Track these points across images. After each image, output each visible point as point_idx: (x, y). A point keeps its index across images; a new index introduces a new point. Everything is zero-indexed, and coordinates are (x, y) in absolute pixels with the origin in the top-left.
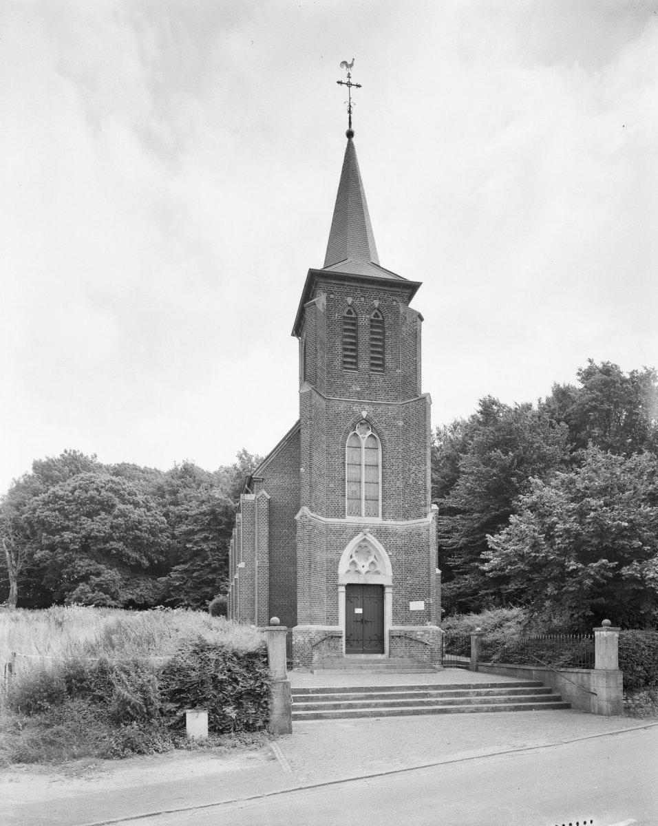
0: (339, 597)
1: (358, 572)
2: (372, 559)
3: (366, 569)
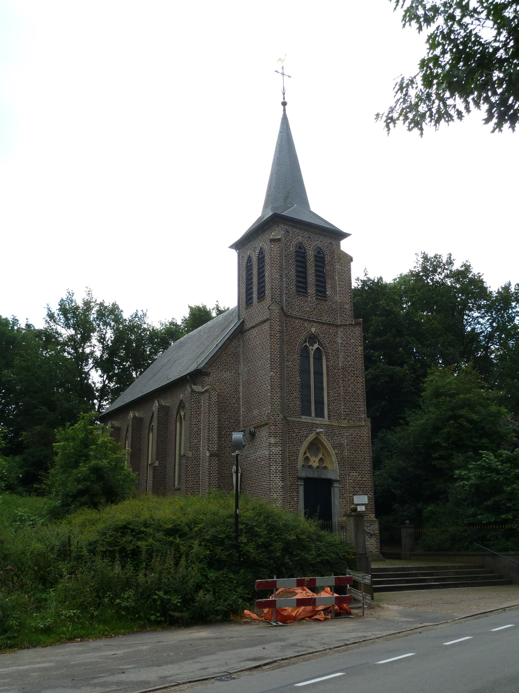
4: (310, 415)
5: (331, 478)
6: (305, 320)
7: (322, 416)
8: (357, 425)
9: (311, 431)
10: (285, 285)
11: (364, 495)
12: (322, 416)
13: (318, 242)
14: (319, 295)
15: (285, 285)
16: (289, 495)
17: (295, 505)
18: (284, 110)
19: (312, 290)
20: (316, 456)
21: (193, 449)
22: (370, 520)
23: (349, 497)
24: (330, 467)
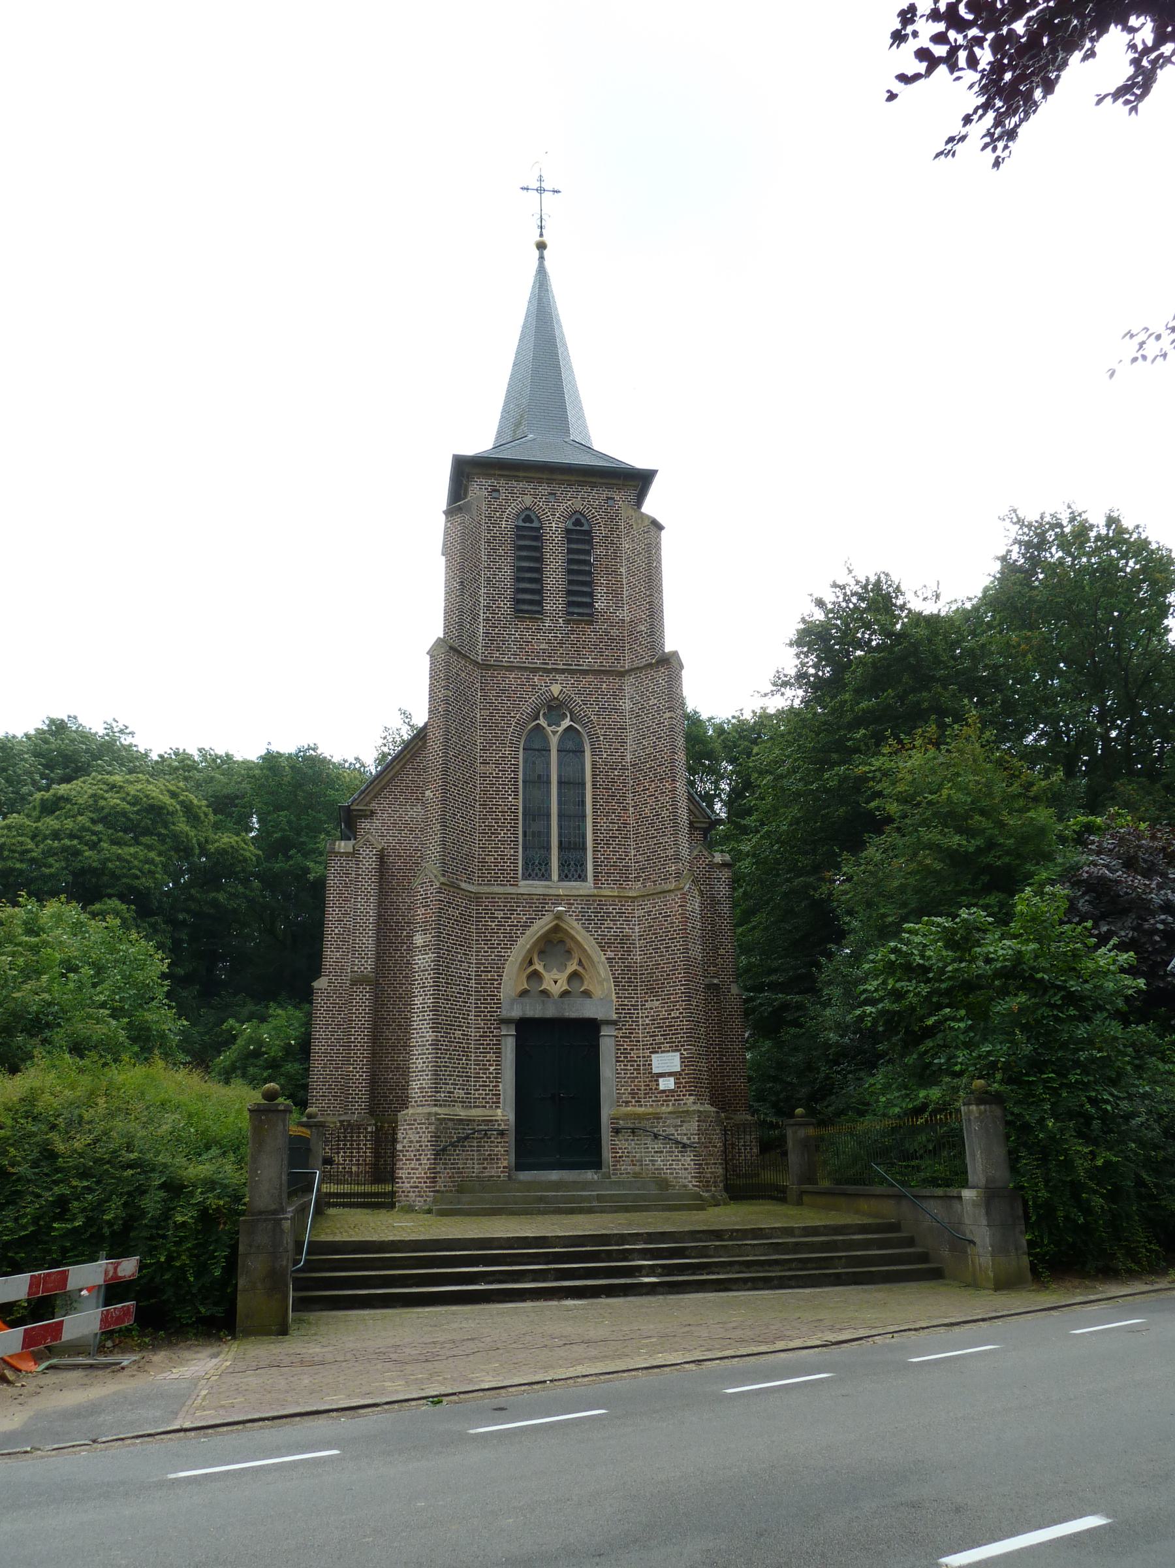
0: (503, 1047)
1: (545, 993)
2: (573, 967)
3: (562, 985)
4: (546, 876)
5: (592, 1016)
6: (534, 670)
8: (659, 890)
9: (540, 912)
10: (483, 603)
11: (673, 1051)
12: (582, 877)
13: (574, 500)
14: (574, 613)
15: (483, 603)
16: (475, 1060)
18: (542, 258)
19: (554, 603)
20: (562, 967)
22: (683, 1112)
23: (644, 1057)
24: (597, 992)
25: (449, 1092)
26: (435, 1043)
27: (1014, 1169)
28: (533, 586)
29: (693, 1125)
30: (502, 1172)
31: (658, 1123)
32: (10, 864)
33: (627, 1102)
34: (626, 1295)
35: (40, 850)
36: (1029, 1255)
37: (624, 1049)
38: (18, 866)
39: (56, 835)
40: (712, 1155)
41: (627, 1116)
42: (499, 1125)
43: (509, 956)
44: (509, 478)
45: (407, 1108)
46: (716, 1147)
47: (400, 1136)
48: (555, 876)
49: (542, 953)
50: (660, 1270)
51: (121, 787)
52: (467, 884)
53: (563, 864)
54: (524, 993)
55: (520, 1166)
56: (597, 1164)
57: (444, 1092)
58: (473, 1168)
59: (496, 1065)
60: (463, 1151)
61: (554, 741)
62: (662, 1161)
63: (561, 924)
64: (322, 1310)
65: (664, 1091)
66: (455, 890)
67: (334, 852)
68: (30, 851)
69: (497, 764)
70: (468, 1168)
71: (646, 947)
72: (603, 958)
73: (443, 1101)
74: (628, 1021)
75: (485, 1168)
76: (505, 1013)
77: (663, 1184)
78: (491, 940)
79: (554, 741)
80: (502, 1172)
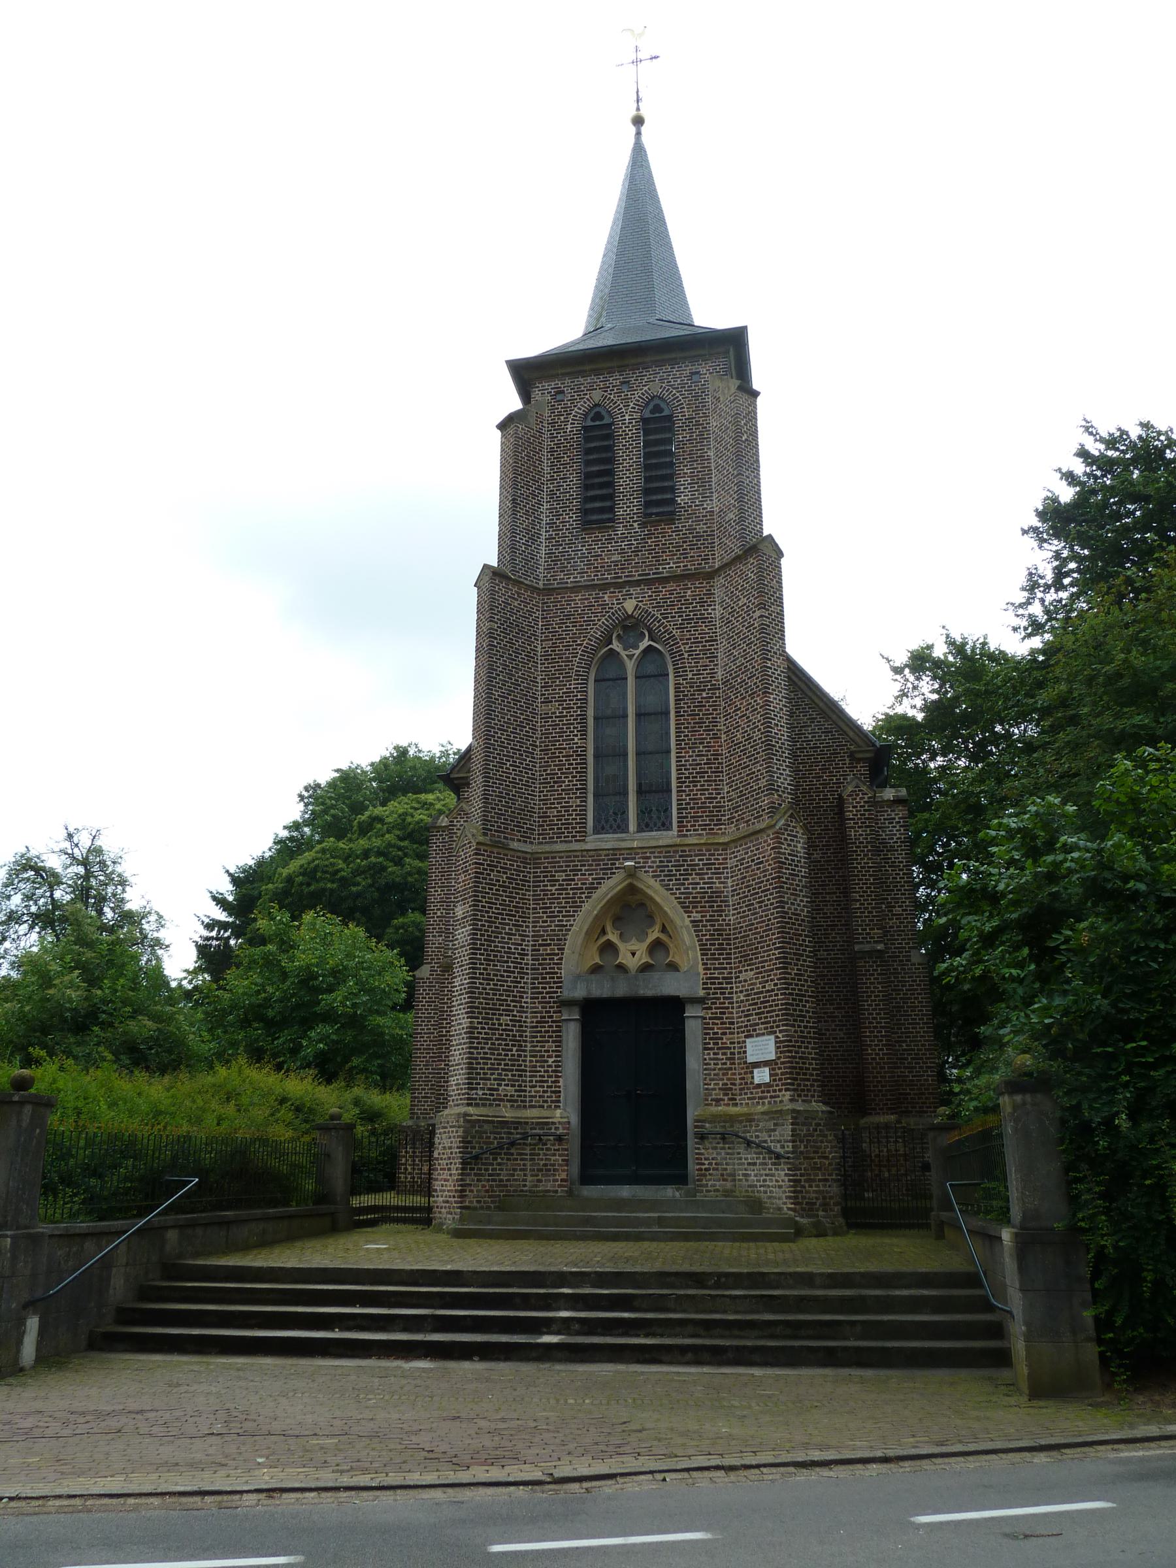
0: (564, 1034)
1: (621, 968)
2: (654, 934)
3: (642, 957)
4: (622, 828)
6: (604, 587)
7: (663, 824)
8: (751, 831)
9: (609, 871)
12: (666, 826)
14: (652, 514)
16: (531, 1051)
17: (549, 1076)
18: (638, 134)
19: (628, 506)
20: (642, 937)
21: (432, 959)
22: (776, 1112)
23: (739, 1043)
25: (489, 1089)
26: (471, 1030)
27: (1073, 1200)
28: (604, 492)
29: (787, 1130)
30: (560, 1186)
31: (751, 1126)
32: (322, 884)
33: (718, 1101)
34: (507, 1359)
35: (350, 870)
36: (1100, 1341)
37: (714, 1033)
38: (329, 885)
39: (366, 854)
40: (819, 1169)
41: (714, 1118)
42: (557, 1129)
43: (571, 925)
44: (573, 375)
45: (446, 1108)
46: (826, 1158)
47: (436, 1141)
48: (632, 827)
49: (618, 920)
50: (577, 1326)
51: (431, 804)
52: (522, 844)
53: (642, 812)
54: (596, 969)
55: (586, 1179)
56: (681, 1179)
57: (483, 1089)
58: (525, 1180)
59: (556, 1056)
60: (508, 1159)
61: (630, 666)
62: (756, 1176)
63: (635, 883)
64: (126, 1351)
65: (759, 1086)
66: (500, 850)
67: (435, 827)
68: (342, 870)
69: (561, 701)
70: (516, 1180)
71: (739, 903)
72: (687, 921)
73: (481, 1099)
74: (719, 999)
75: (539, 1181)
76: (567, 993)
77: (755, 1205)
78: (551, 908)
79: (630, 666)
80: (560, 1186)
